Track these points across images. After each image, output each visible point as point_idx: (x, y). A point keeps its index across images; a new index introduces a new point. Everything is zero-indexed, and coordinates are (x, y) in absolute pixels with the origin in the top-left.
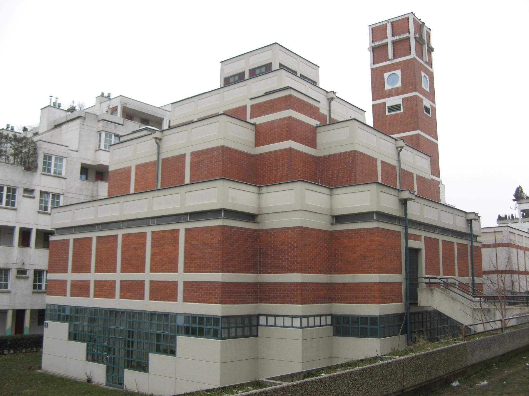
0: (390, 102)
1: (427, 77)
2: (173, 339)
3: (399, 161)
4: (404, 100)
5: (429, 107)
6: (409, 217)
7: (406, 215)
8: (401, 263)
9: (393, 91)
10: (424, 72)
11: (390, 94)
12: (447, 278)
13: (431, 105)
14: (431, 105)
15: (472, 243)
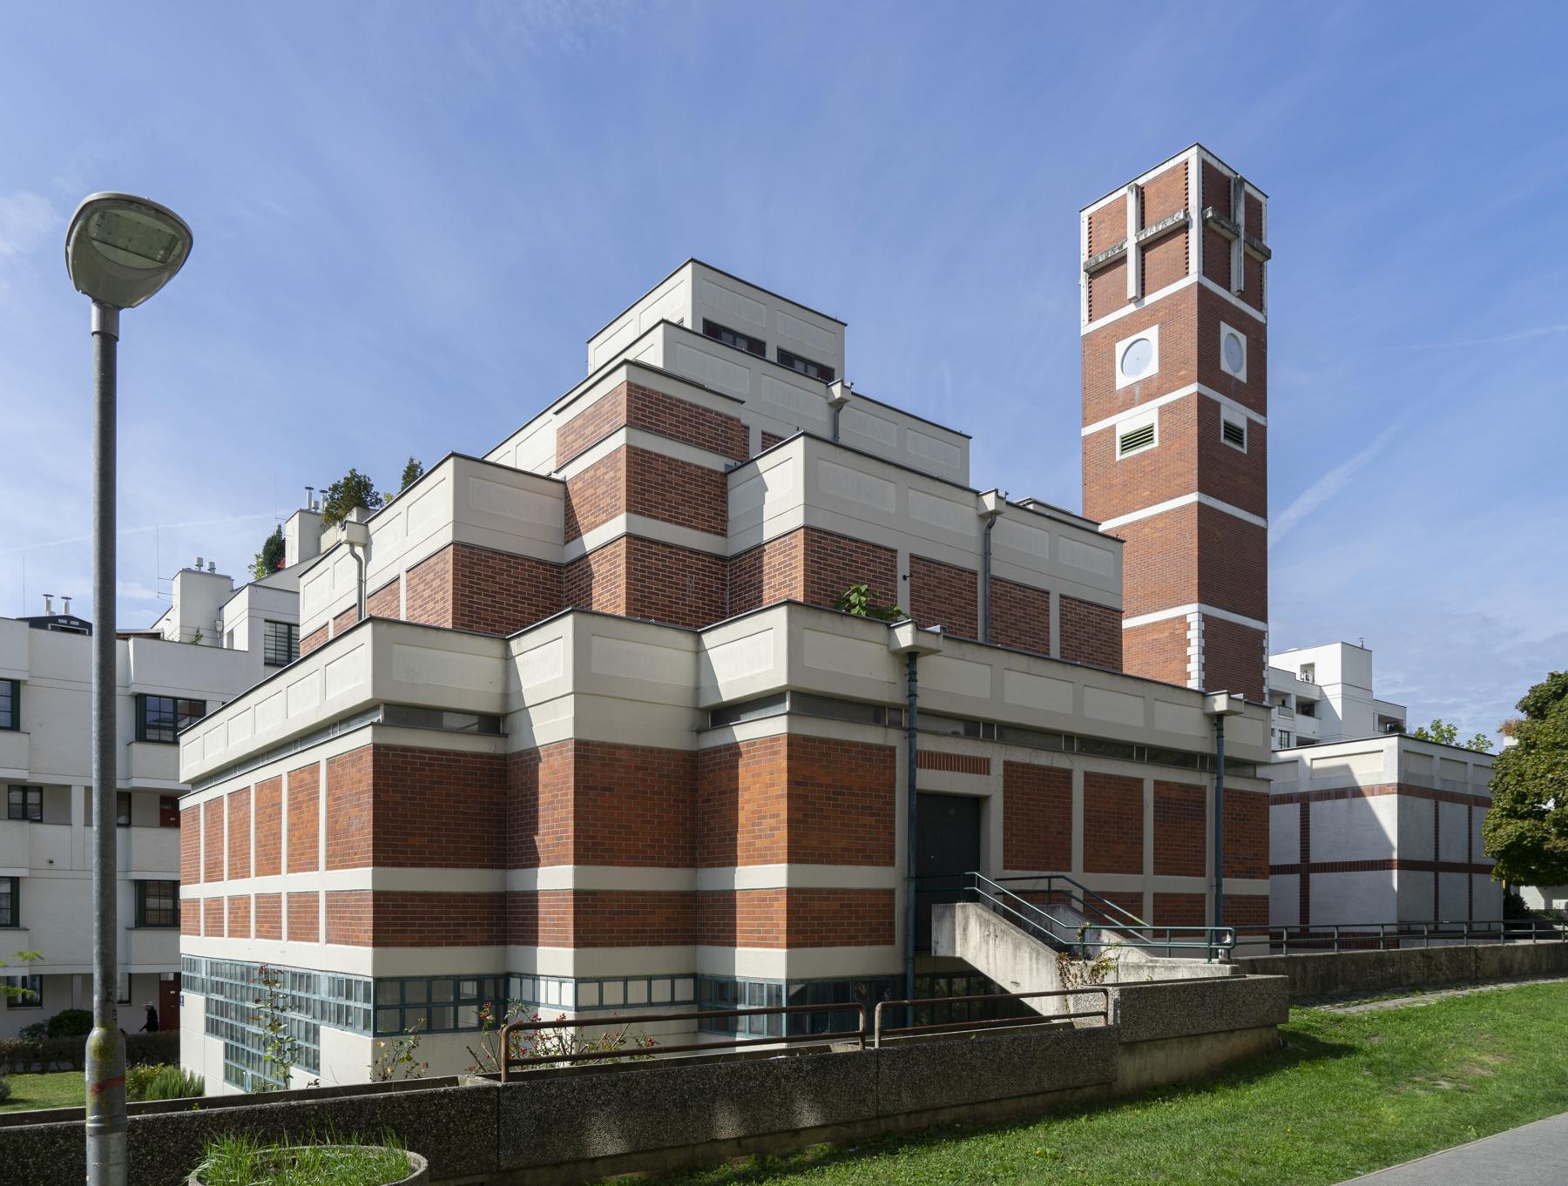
0: (1127, 422)
1: (1243, 338)
2: (313, 1033)
3: (986, 554)
4: (1163, 410)
5: (1241, 423)
6: (923, 702)
7: (912, 695)
8: (893, 834)
9: (1137, 390)
10: (1231, 324)
11: (1130, 400)
12: (1049, 878)
13: (1249, 421)
14: (1249, 421)
15: (1219, 779)
